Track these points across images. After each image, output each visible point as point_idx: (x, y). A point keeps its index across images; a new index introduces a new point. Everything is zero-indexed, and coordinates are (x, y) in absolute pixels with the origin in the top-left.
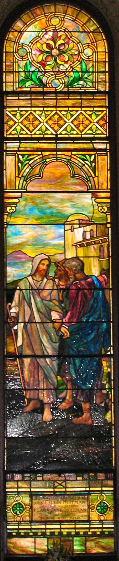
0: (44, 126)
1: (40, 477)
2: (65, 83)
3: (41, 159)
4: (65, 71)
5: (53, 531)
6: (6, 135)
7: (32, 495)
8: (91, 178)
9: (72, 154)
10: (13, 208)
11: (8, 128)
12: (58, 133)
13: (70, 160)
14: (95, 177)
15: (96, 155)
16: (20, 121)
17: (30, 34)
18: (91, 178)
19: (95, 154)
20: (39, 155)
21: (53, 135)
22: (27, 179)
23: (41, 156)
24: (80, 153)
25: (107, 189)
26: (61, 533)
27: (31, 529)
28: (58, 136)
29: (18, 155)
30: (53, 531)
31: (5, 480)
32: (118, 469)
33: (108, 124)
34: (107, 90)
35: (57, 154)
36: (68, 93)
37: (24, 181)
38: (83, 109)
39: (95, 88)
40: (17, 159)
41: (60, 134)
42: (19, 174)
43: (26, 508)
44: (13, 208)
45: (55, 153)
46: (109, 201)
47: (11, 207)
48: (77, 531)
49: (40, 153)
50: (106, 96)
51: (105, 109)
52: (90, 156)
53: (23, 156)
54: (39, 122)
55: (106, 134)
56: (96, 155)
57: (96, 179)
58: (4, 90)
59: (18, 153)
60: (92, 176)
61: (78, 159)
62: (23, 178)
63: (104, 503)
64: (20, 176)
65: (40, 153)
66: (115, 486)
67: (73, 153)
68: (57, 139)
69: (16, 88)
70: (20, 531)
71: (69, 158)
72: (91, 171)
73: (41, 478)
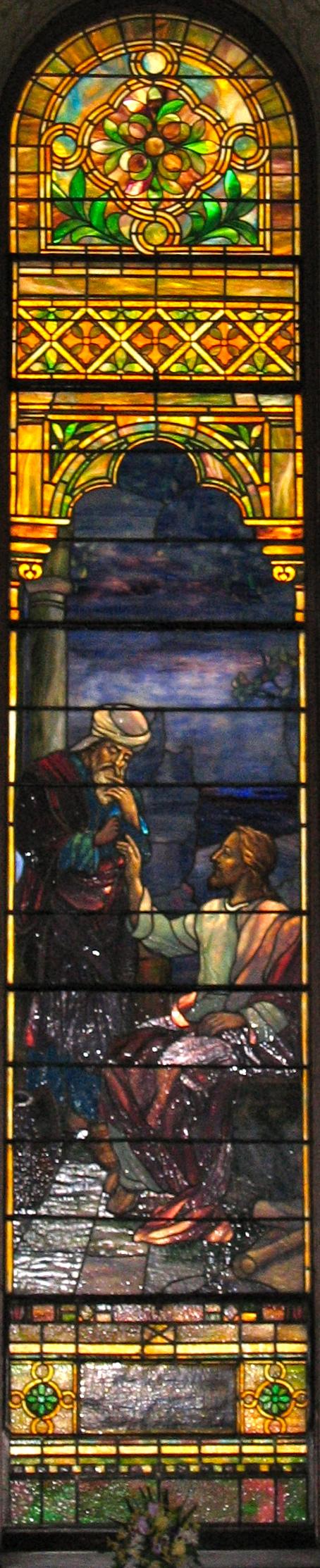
0: (124, 351)
1: (70, 1312)
2: (180, 234)
3: (114, 436)
4: (184, 199)
5: (256, 1460)
6: (18, 373)
7: (78, 1360)
8: (251, 488)
9: (199, 423)
10: (35, 567)
11: (21, 354)
12: (162, 368)
13: (194, 438)
14: (263, 484)
15: (267, 426)
16: (47, 345)
17: (87, 105)
18: (251, 488)
19: (262, 424)
20: (109, 423)
21: (148, 374)
22: (74, 489)
23: (113, 427)
24: (227, 419)
25: (296, 518)
26: (159, 1472)
27: (77, 1456)
28: (161, 378)
29: (52, 422)
30: (256, 1460)
31: (8, 1321)
32: (317, 1295)
33: (298, 347)
34: (297, 252)
35: (157, 422)
36: (188, 261)
37: (65, 494)
38: (229, 305)
39: (264, 246)
40: (47, 436)
41: (167, 372)
42: (52, 474)
43: (64, 1397)
44: (35, 567)
45: (152, 418)
46: (299, 550)
47: (31, 564)
48: (206, 1460)
49: (110, 418)
50: (293, 270)
51: (290, 306)
52: (250, 426)
53: (64, 425)
54: (108, 341)
55: (293, 375)
56: (267, 426)
57: (265, 494)
58: (13, 250)
59: (50, 417)
60: (252, 482)
61: (216, 436)
62: (62, 487)
63: (282, 1386)
64: (56, 479)
65: (110, 418)
66: (311, 1341)
67: (203, 419)
68: (155, 385)
69: (47, 244)
70: (281, 1460)
71: (192, 433)
72: (251, 469)
73: (106, 1317)
